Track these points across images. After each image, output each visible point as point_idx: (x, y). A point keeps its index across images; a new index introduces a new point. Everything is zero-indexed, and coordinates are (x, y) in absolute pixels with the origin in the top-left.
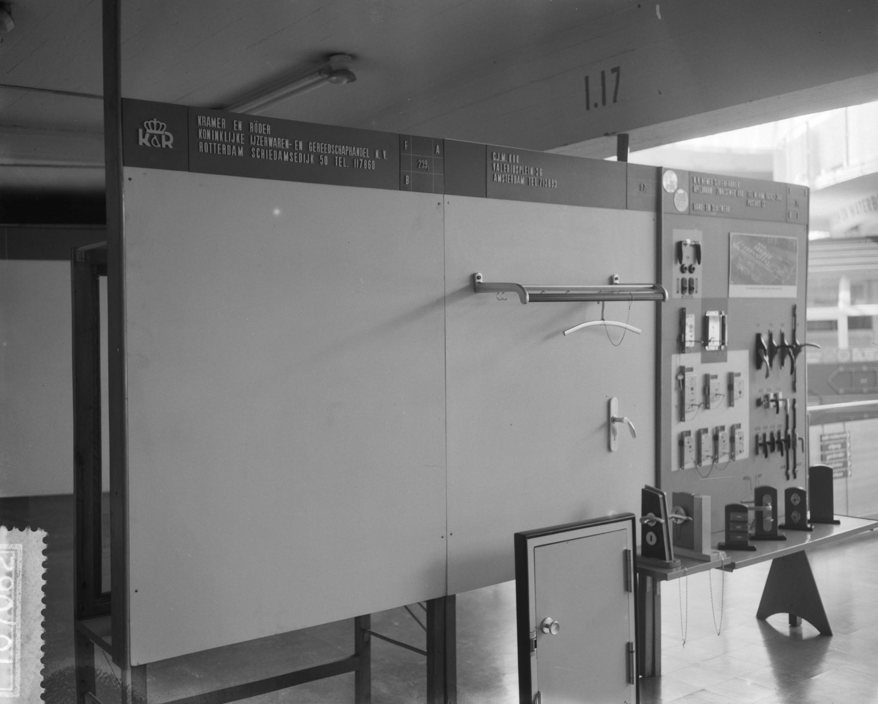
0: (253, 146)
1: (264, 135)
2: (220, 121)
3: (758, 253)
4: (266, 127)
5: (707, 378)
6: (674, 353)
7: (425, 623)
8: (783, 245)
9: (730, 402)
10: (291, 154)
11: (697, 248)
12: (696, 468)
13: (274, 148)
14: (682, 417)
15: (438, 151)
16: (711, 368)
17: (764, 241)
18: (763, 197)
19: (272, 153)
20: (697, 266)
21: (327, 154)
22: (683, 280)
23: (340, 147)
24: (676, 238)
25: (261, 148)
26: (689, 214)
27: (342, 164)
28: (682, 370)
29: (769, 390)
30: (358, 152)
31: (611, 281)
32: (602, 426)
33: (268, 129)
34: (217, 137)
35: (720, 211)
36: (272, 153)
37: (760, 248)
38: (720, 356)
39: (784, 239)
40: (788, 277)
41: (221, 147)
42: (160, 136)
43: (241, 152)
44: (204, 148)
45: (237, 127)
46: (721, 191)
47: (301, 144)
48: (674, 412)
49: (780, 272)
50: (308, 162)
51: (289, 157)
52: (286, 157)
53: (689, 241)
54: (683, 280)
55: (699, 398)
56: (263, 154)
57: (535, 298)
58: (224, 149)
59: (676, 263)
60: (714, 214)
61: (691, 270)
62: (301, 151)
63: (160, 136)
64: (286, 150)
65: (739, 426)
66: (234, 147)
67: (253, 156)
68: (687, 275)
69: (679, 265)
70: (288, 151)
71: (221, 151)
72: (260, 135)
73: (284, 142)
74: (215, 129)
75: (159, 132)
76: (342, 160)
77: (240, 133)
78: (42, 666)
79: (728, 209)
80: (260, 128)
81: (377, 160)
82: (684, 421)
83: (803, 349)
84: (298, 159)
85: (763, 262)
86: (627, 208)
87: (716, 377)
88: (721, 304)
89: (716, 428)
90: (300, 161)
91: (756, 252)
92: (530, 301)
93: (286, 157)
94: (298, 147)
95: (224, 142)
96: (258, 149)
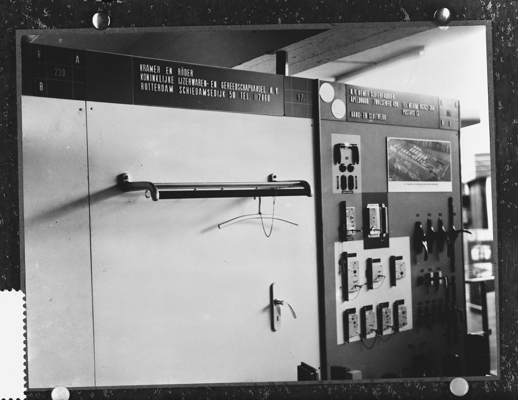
0: (180, 85)
1: (188, 77)
2: (156, 68)
3: (414, 155)
4: (189, 71)
5: (370, 262)
6: (336, 241)
8: (437, 147)
9: (393, 283)
10: (208, 90)
11: (354, 149)
13: (195, 87)
14: (345, 297)
15: (78, 61)
16: (373, 253)
17: (420, 144)
18: (417, 107)
19: (194, 90)
20: (356, 166)
21: (235, 91)
22: (343, 178)
23: (244, 85)
24: (334, 142)
25: (186, 86)
26: (347, 121)
27: (246, 97)
28: (345, 256)
29: (430, 270)
30: (257, 89)
31: (270, 178)
32: (265, 309)
33: (192, 73)
34: (154, 79)
35: (377, 119)
36: (194, 90)
37: (416, 150)
38: (382, 242)
39: (437, 143)
40: (443, 175)
41: (157, 86)
43: (171, 90)
45: (169, 72)
46: (377, 102)
47: (215, 83)
48: (339, 293)
49: (435, 170)
50: (220, 96)
51: (207, 93)
52: (205, 93)
53: (347, 145)
54: (343, 178)
55: (362, 279)
56: (188, 91)
57: (164, 196)
58: (159, 88)
59: (335, 164)
60: (371, 121)
61: (351, 168)
62: (215, 89)
64: (205, 88)
65: (402, 302)
66: (166, 86)
67: (181, 92)
68: (347, 174)
69: (338, 165)
70: (206, 88)
71: (157, 89)
72: (186, 77)
73: (203, 82)
74: (152, 73)
76: (246, 94)
77: (171, 76)
79: (384, 117)
80: (185, 72)
81: (271, 95)
82: (347, 300)
83: (460, 234)
84: (213, 94)
85: (419, 162)
87: (400, 258)
88: (382, 198)
89: (380, 304)
90: (215, 96)
91: (412, 154)
92: (160, 198)
93: (205, 93)
94: (213, 86)
95: (158, 83)
96: (184, 87)
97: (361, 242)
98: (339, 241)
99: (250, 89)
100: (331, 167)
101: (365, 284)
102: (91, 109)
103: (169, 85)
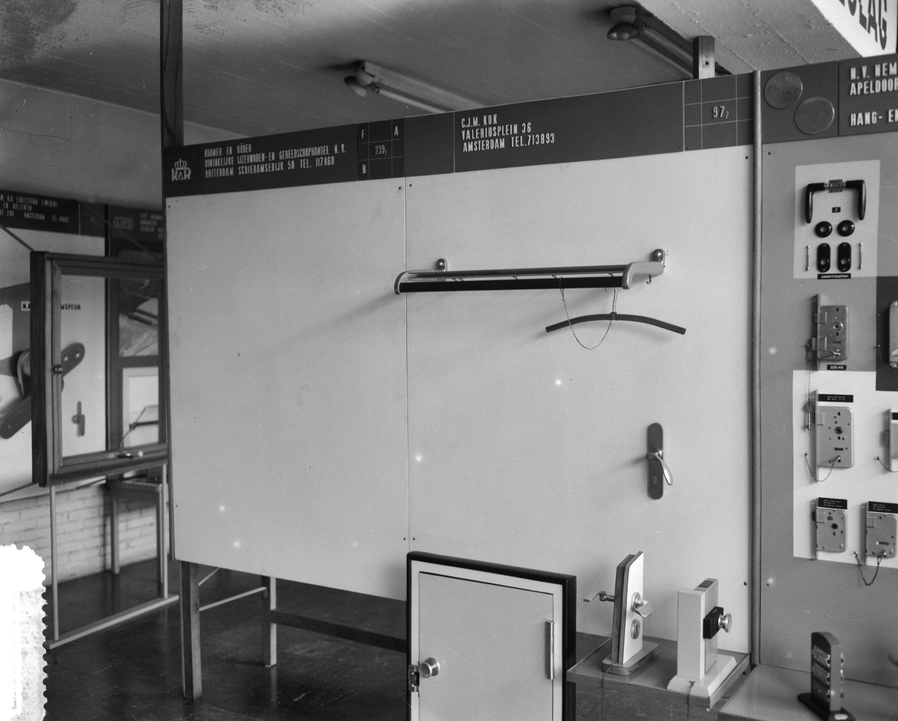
7: (141, 353)
12: (859, 565)
14: (814, 477)
15: (396, 133)
30: (317, 151)
42: (183, 171)
44: (208, 174)
51: (474, 147)
54: (823, 251)
61: (845, 229)
63: (183, 171)
76: (519, 139)
78: (45, 700)
97: (872, 376)
98: (807, 369)
99: (501, 132)
101: (637, 461)
102: (769, 153)
103: (229, 166)
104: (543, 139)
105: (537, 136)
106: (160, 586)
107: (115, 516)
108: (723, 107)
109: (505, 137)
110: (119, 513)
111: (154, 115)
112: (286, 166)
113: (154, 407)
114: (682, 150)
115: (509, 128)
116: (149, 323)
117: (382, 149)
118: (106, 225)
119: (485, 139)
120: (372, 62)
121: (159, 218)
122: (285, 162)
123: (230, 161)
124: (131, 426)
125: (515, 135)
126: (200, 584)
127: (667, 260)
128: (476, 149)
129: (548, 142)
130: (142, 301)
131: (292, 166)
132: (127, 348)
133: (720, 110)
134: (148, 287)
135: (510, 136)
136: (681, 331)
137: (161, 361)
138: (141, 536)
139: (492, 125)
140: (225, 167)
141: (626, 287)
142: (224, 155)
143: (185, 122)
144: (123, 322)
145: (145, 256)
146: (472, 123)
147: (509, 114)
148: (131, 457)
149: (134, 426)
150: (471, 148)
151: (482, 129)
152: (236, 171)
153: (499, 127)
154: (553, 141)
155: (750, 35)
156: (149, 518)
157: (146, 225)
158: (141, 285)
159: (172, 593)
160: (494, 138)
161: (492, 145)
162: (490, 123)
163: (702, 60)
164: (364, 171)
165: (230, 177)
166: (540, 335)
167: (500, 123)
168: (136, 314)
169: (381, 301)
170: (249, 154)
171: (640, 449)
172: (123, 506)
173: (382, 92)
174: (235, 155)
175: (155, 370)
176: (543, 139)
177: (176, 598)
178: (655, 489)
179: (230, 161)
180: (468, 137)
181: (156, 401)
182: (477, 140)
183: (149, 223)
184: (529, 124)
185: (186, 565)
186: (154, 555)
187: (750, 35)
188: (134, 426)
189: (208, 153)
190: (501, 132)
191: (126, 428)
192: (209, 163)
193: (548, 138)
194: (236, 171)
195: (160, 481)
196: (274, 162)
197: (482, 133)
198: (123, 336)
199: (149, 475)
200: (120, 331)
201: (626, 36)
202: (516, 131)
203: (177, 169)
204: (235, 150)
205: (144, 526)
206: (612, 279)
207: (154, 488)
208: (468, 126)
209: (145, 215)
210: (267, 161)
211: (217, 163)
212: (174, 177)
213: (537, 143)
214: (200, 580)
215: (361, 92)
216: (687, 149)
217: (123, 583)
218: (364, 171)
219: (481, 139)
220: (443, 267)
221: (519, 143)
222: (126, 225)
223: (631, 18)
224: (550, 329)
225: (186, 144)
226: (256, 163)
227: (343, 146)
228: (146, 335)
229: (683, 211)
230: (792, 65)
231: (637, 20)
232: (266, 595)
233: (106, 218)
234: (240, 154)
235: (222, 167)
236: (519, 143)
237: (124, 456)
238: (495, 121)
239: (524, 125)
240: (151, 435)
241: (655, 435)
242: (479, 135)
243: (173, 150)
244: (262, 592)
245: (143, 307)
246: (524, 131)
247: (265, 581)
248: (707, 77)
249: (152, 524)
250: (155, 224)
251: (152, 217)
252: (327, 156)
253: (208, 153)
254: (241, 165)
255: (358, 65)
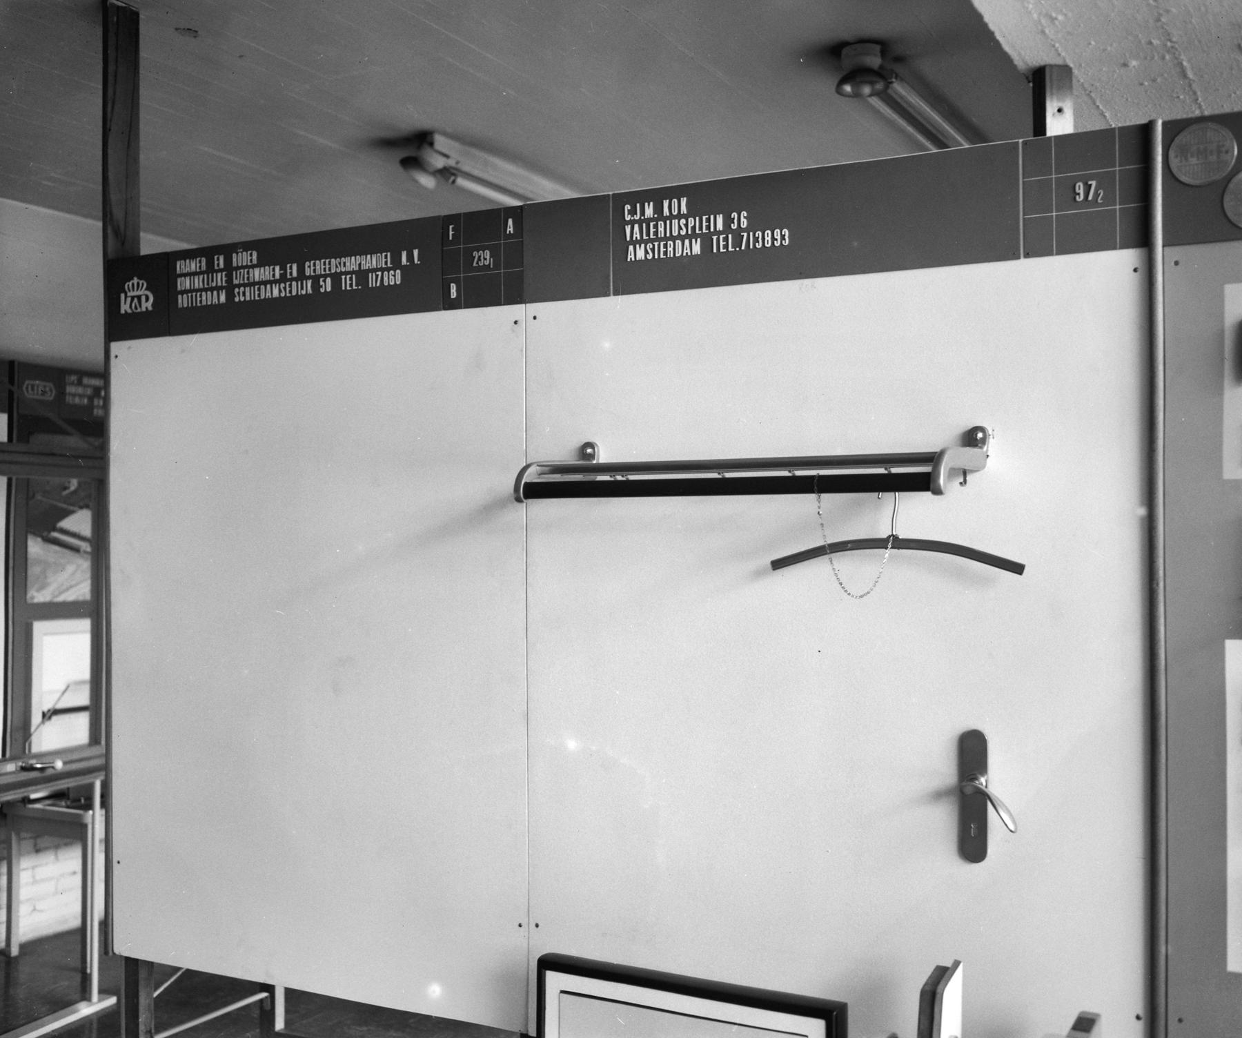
7: (61, 599)
15: (510, 229)
19: (666, 246)
41: (666, 246)
42: (139, 297)
44: (183, 301)
47: (295, 267)
51: (280, 291)
66: (687, 242)
75: (139, 293)
76: (726, 239)
86: (12, 364)
90: (294, 293)
99: (694, 228)
100: (1220, 392)
101: (938, 795)
102: (1176, 263)
103: (218, 289)
104: (768, 238)
105: (759, 234)
106: (86, 979)
107: (14, 861)
108: (1093, 183)
109: (702, 235)
110: (20, 854)
111: (89, 221)
112: (316, 286)
113: (83, 682)
114: (1019, 258)
115: (708, 220)
116: (76, 550)
117: (485, 258)
118: (11, 393)
119: (666, 239)
120: (445, 134)
121: (97, 382)
122: (316, 279)
123: (220, 279)
124: (44, 715)
125: (719, 233)
126: (156, 994)
127: (992, 446)
128: (650, 257)
129: (777, 244)
130: (66, 514)
131: (327, 286)
132: (38, 590)
133: (1088, 188)
134: (75, 492)
135: (710, 235)
136: (1017, 568)
137: (96, 610)
138: (56, 893)
139: (679, 216)
140: (212, 289)
141: (938, 492)
142: (211, 269)
143: (142, 234)
144: (35, 547)
145: (74, 442)
146: (643, 213)
147: (704, 197)
148: (42, 769)
149: (47, 716)
150: (641, 254)
151: (661, 223)
152: (230, 296)
153: (691, 220)
154: (786, 242)
155: (1134, 63)
156: (70, 860)
157: (76, 394)
158: (65, 488)
159: (104, 992)
160: (682, 238)
161: (679, 249)
162: (675, 212)
163: (1051, 107)
164: (454, 294)
165: (220, 305)
166: (758, 574)
167: (692, 212)
168: (55, 535)
169: (489, 510)
170: (253, 267)
171: (945, 770)
172: (27, 844)
173: (461, 181)
174: (229, 269)
175: (86, 624)
176: (768, 238)
177: (112, 1001)
178: (972, 844)
179: (220, 279)
180: (637, 235)
181: (86, 674)
182: (652, 241)
183: (80, 390)
184: (744, 214)
185: (132, 964)
186: (76, 923)
187: (1134, 63)
188: (47, 716)
189: (181, 266)
190: (694, 228)
191: (36, 718)
192: (184, 283)
193: (778, 237)
194: (230, 296)
195: (89, 806)
196: (296, 279)
197: (661, 229)
198: (33, 571)
199: (71, 795)
200: (29, 562)
201: (867, 90)
202: (720, 226)
203: (130, 294)
204: (228, 261)
205: (62, 875)
206: (914, 475)
207: (79, 816)
208: (637, 217)
209: (74, 378)
210: (283, 278)
211: (198, 282)
212: (125, 308)
213: (759, 245)
214: (156, 989)
215: (427, 181)
216: (1027, 255)
217: (23, 972)
218: (454, 294)
219: (659, 240)
220: (592, 456)
221: (726, 246)
222: (44, 393)
223: (874, 61)
224: (778, 564)
225: (143, 253)
226: (263, 280)
227: (416, 252)
228: (70, 569)
229: (1021, 361)
230: (1227, 109)
231: (881, 67)
232: (268, 1007)
233: (12, 381)
234: (238, 268)
235: (206, 290)
236: (726, 246)
237: (32, 769)
238: (684, 210)
239: (735, 215)
240: (76, 731)
241: (972, 751)
242: (656, 233)
243: (121, 265)
244: (261, 1001)
245: (66, 524)
246: (734, 226)
247: (269, 989)
248: (1060, 133)
249: (75, 873)
250: (89, 392)
251: (86, 381)
252: (388, 270)
253: (181, 266)
254: (239, 286)
255: (423, 138)
